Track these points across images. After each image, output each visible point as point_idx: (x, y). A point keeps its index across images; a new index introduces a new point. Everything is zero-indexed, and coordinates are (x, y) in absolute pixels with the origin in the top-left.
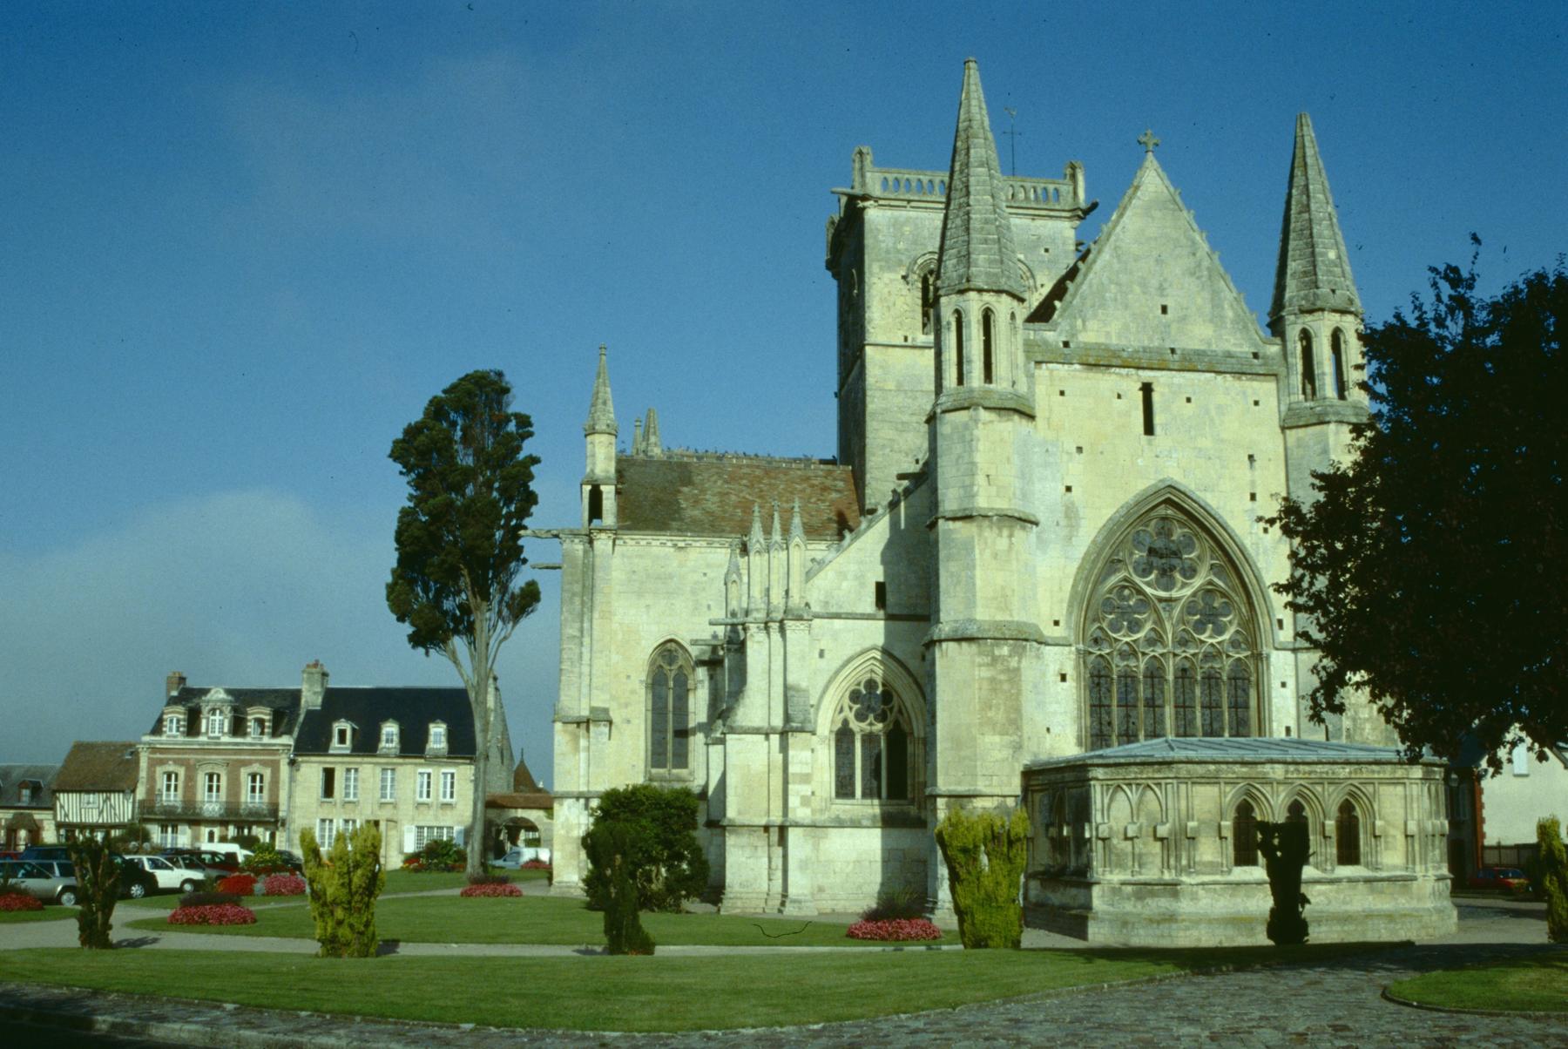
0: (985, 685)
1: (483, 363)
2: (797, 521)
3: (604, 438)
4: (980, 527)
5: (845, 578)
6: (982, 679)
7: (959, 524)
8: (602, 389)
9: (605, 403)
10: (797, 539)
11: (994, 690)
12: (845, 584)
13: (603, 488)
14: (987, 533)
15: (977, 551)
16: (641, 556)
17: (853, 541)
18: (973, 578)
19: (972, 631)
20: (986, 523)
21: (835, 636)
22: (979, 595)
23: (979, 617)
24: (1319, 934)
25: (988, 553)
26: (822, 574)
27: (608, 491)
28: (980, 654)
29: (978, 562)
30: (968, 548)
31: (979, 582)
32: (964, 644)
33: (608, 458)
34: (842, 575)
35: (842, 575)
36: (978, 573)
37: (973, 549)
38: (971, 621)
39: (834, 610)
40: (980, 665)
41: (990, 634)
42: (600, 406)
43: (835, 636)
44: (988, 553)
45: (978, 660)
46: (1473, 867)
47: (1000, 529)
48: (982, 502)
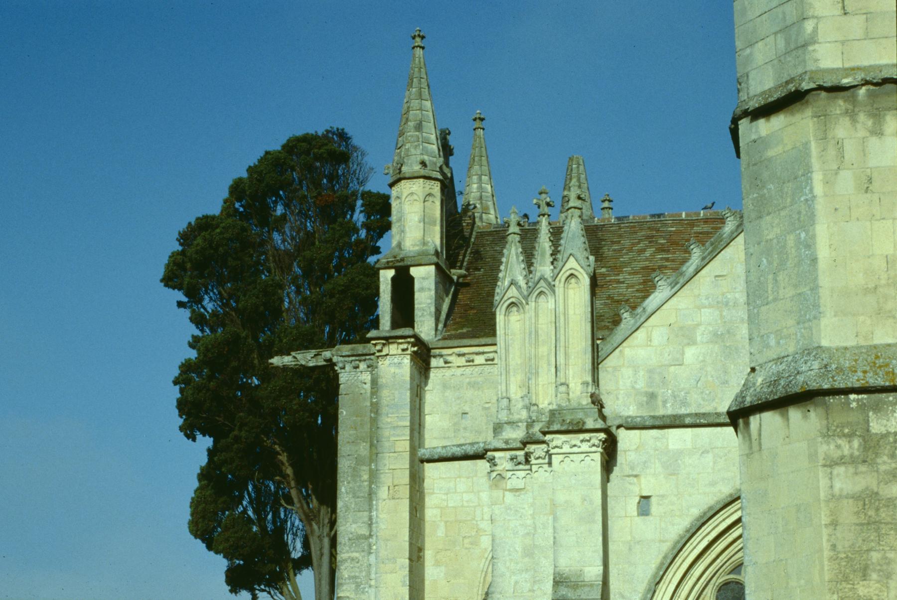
0: (848, 513)
1: (315, 124)
2: (573, 227)
3: (417, 187)
4: (823, 117)
5: (692, 342)
6: (834, 498)
7: (778, 121)
8: (415, 103)
9: (419, 127)
10: (572, 263)
11: (872, 524)
12: (691, 354)
13: (413, 271)
14: (842, 130)
15: (817, 178)
16: (473, 385)
17: (706, 261)
18: (809, 244)
19: (810, 376)
20: (840, 104)
21: (672, 464)
22: (824, 281)
23: (825, 343)
24: (430, 469)
25: (846, 181)
26: (640, 335)
27: (424, 277)
28: (827, 434)
29: (821, 207)
30: (798, 172)
31: (823, 252)
32: (794, 413)
33: (425, 220)
34: (685, 335)
35: (685, 335)
36: (822, 230)
37: (808, 172)
38: (812, 351)
39: (670, 410)
40: (831, 463)
41: (854, 381)
42: (411, 133)
43: (672, 464)
44: (846, 181)
45: (826, 449)
46: (354, 194)
47: (877, 116)
48: (826, 60)
